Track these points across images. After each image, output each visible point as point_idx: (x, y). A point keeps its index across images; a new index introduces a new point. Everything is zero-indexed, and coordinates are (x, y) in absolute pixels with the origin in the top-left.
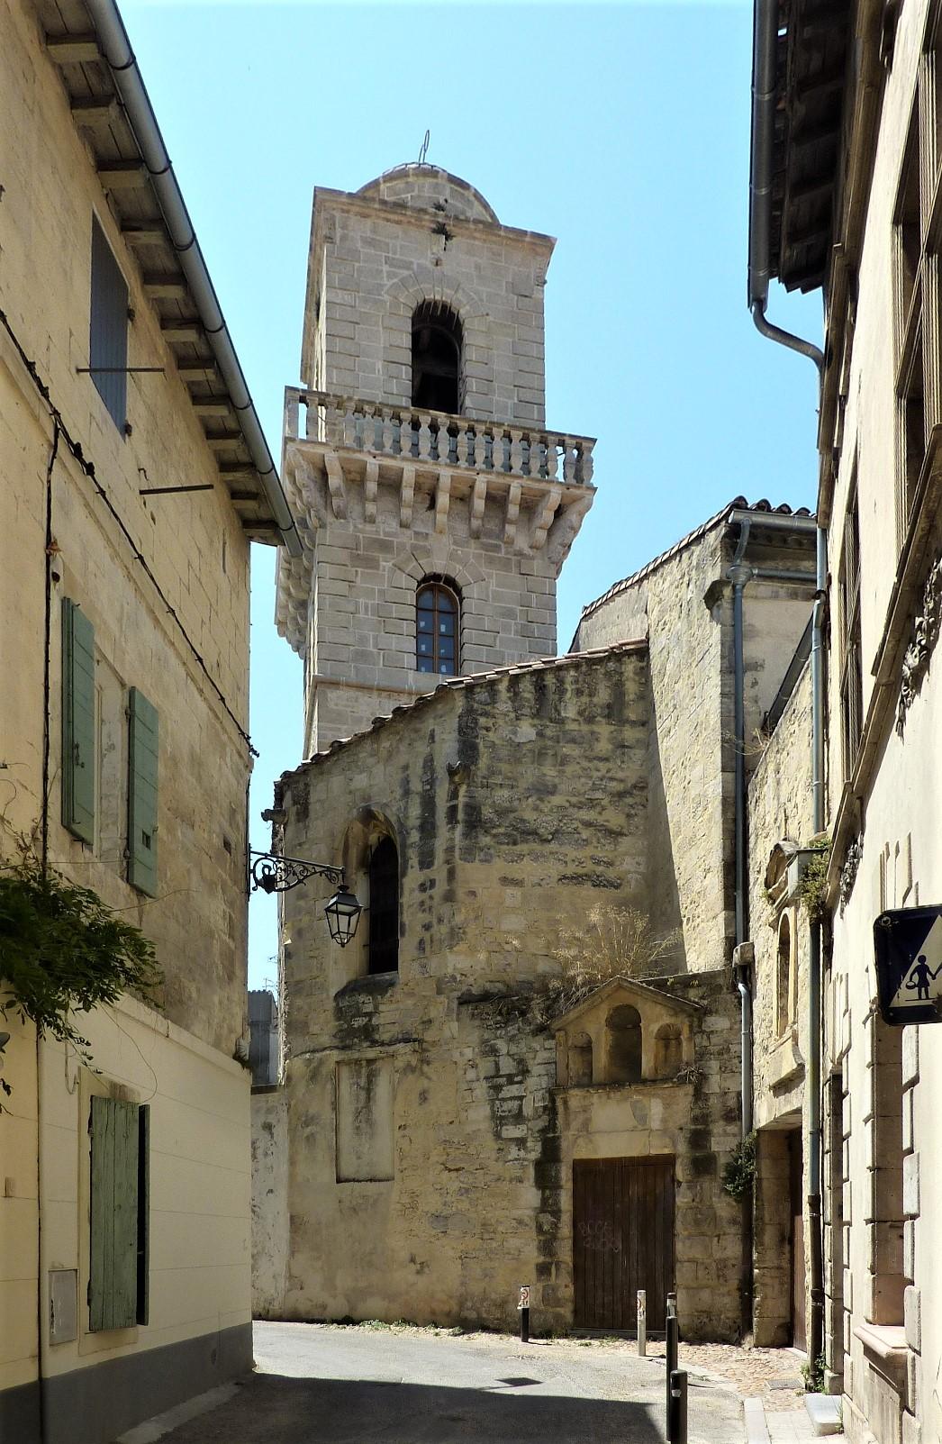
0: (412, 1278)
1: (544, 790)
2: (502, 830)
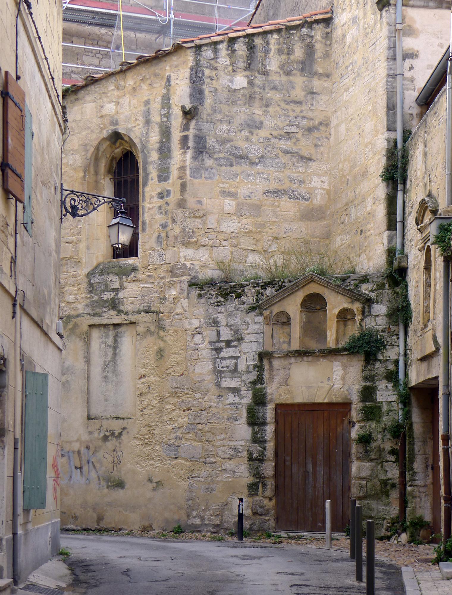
0: (149, 494)
1: (254, 126)
2: (221, 155)
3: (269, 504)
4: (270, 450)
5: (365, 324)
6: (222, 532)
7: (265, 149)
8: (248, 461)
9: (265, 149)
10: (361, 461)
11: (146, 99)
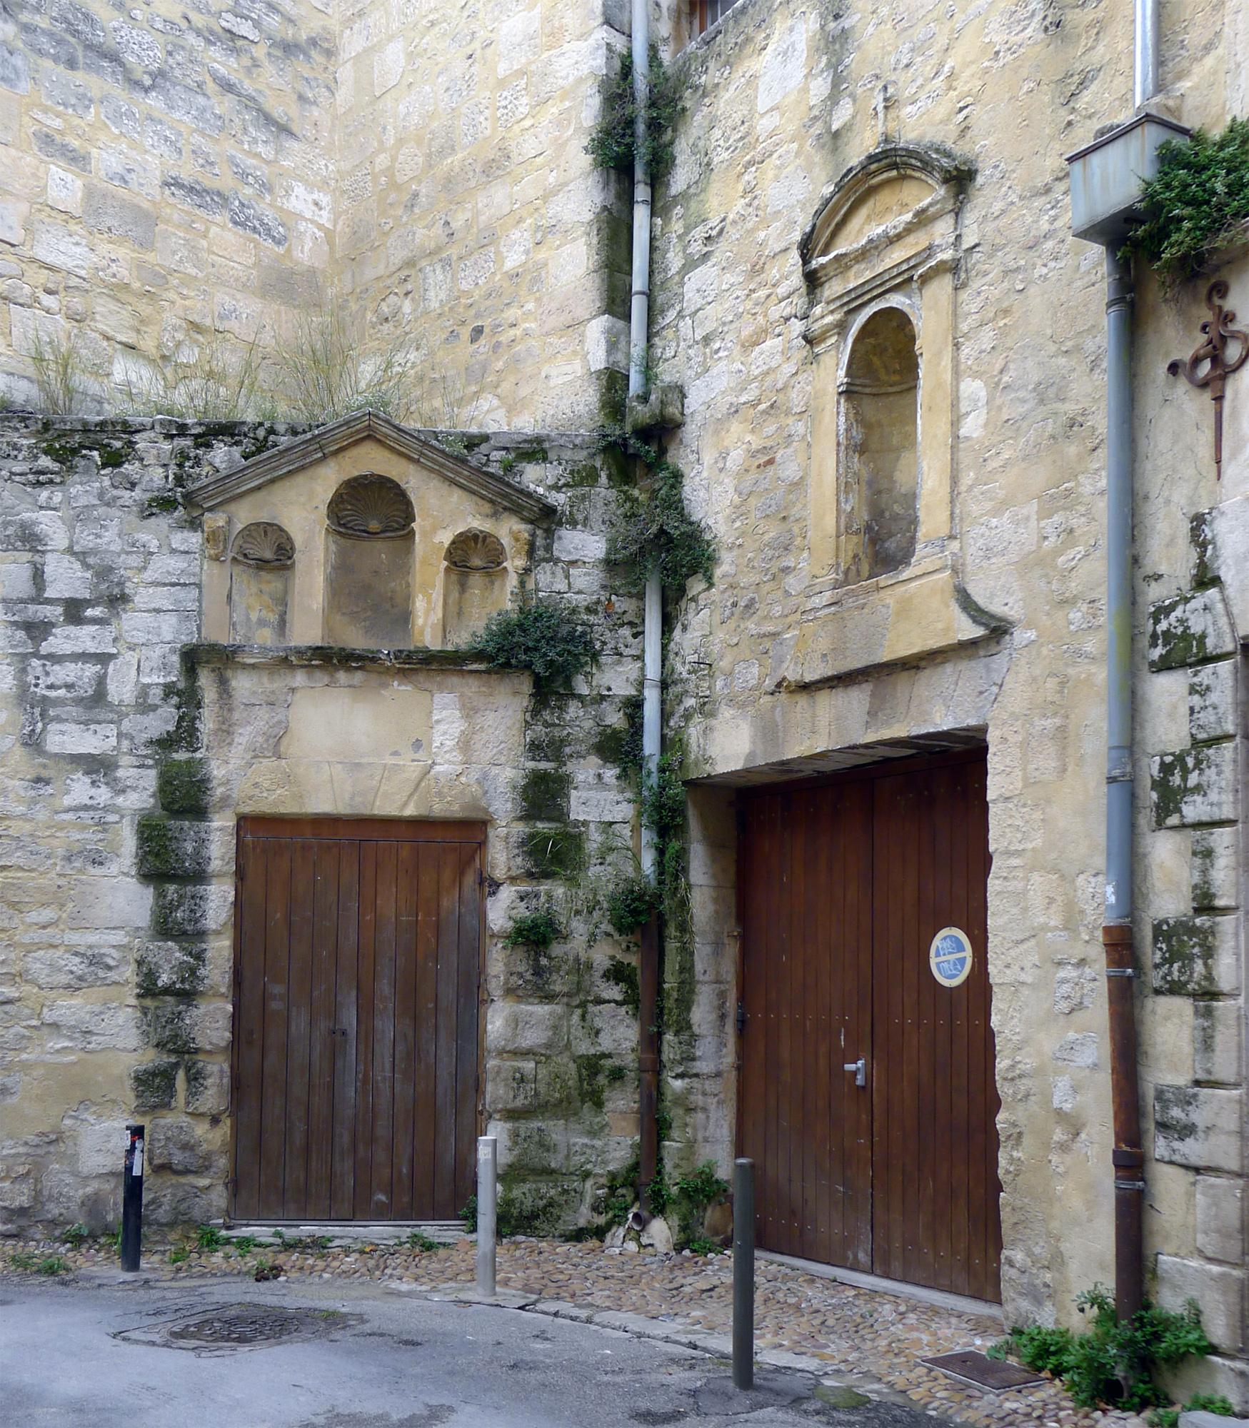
3: (210, 1136)
4: (220, 962)
5: (537, 584)
6: (38, 1232)
8: (139, 996)
9: (170, 53)
10: (520, 999)
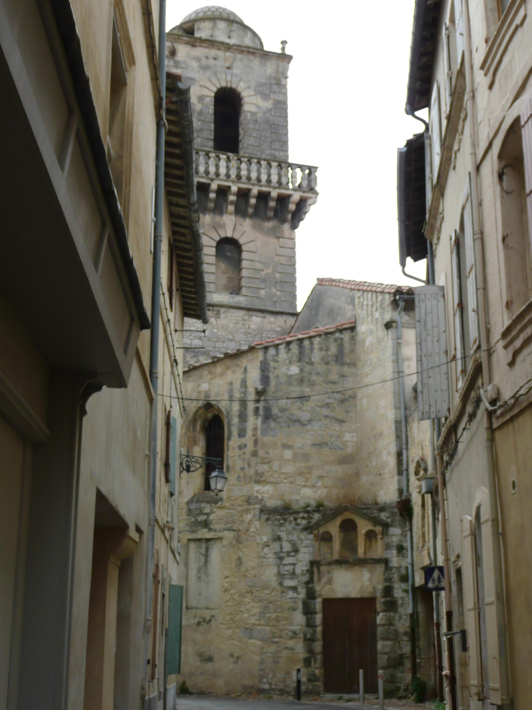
0: (231, 666)
7: (312, 414)
11: (229, 381)
